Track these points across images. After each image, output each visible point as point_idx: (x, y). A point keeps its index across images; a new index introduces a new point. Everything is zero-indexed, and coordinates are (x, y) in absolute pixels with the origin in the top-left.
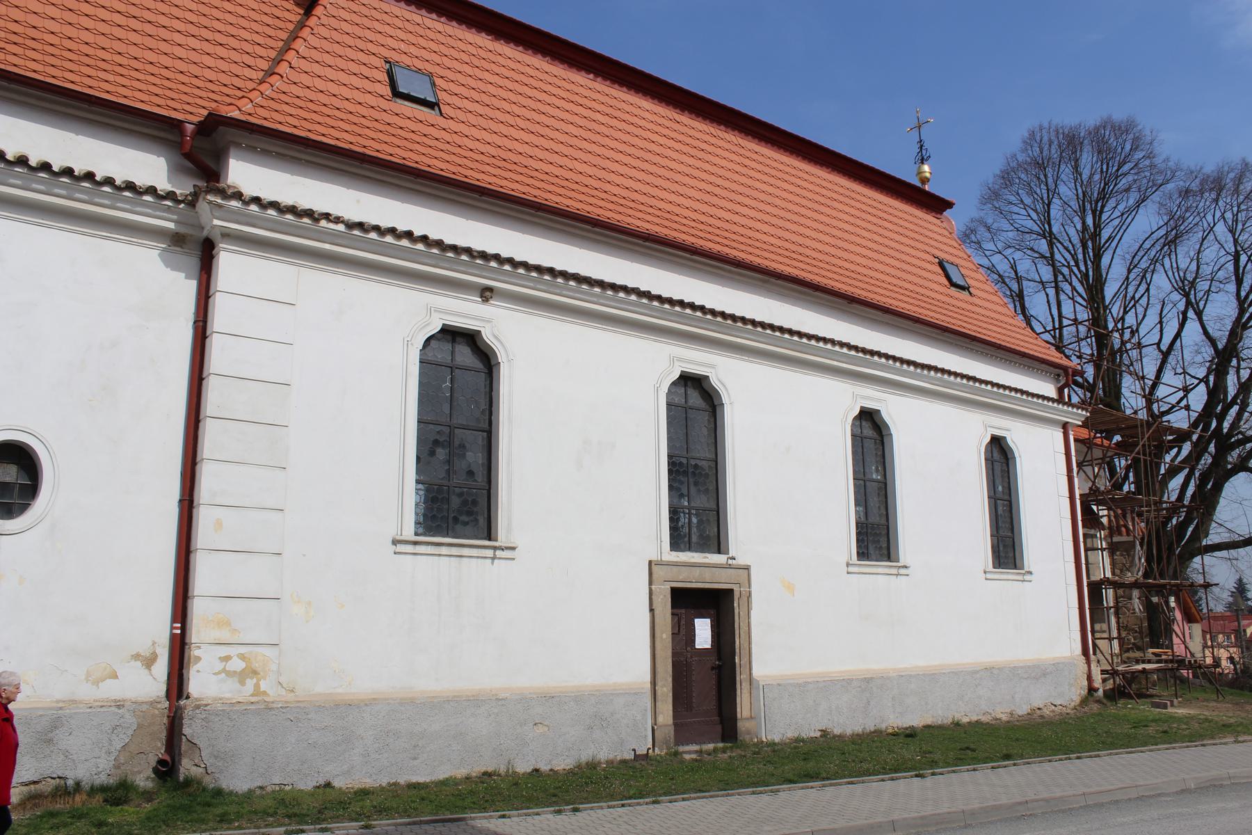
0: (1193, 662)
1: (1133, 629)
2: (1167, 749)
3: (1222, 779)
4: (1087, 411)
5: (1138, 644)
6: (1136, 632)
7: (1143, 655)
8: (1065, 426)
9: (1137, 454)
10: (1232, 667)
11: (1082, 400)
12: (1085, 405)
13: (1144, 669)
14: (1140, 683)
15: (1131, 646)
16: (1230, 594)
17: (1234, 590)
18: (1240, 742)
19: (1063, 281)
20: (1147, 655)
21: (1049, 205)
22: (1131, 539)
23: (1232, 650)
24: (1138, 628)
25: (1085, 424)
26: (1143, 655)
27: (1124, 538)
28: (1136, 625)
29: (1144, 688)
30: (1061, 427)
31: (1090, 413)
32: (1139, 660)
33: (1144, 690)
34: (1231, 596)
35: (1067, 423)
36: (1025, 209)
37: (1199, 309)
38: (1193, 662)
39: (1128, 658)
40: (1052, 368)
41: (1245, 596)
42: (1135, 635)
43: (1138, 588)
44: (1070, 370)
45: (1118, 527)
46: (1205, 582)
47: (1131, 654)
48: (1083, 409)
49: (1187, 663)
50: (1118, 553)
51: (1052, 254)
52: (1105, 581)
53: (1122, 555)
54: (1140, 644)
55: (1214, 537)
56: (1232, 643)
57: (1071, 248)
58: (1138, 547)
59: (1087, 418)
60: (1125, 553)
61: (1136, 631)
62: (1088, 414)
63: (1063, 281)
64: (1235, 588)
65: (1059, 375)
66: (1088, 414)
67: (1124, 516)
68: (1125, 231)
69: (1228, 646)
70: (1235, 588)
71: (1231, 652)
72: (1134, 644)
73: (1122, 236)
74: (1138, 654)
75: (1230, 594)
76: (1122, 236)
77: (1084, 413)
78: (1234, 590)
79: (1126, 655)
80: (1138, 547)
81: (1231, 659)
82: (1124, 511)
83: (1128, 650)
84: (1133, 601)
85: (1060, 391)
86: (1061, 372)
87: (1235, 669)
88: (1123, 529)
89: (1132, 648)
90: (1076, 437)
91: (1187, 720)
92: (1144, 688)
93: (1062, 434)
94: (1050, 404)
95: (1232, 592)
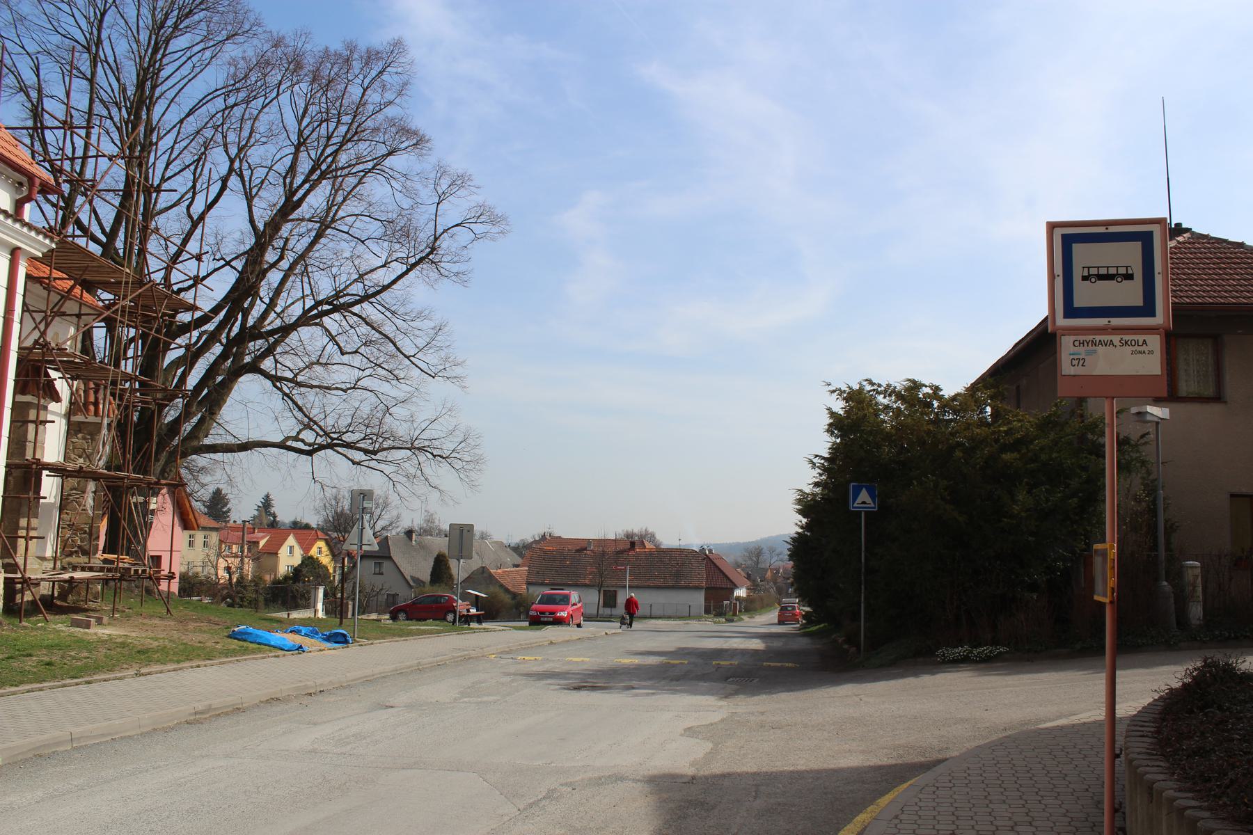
0: (140, 572)
1: (82, 529)
2: (28, 691)
3: (58, 744)
4: (52, 240)
5: (85, 547)
6: (85, 532)
7: (87, 560)
8: (15, 252)
9: (113, 313)
10: (227, 576)
11: (50, 227)
12: (53, 233)
13: (72, 578)
14: (79, 594)
15: (76, 549)
16: (256, 508)
17: (261, 505)
18: (143, 675)
19: (106, 118)
20: (92, 561)
21: (103, 15)
22: (98, 420)
23: (230, 560)
24: (89, 528)
25: (47, 258)
26: (87, 560)
27: (92, 419)
28: (86, 524)
29: (82, 601)
30: (9, 251)
31: (56, 244)
32: (77, 566)
33: (82, 603)
34: (257, 510)
35: (19, 248)
36: (69, 6)
37: (251, 194)
38: (140, 572)
39: (69, 564)
40: (10, 170)
41: (269, 511)
42: (83, 536)
43: (95, 479)
44: (37, 181)
45: (86, 404)
46: (34, 458)
47: (74, 559)
48: (46, 236)
49: (132, 572)
50: (80, 436)
51: (94, 74)
52: (34, 463)
53: (84, 438)
54: (87, 548)
55: (214, 437)
56: (232, 553)
57: (115, 68)
58: (104, 431)
59: (52, 251)
60: (89, 437)
61: (86, 531)
62: (54, 246)
63: (106, 118)
64: (262, 502)
65: (21, 184)
66: (54, 246)
67: (96, 392)
68: (190, 81)
69: (228, 557)
70: (262, 502)
71: (230, 562)
72: (79, 547)
73: (185, 85)
74: (83, 560)
75: (256, 508)
76: (185, 85)
77: (47, 241)
78: (261, 505)
79: (68, 559)
80: (104, 431)
81: (228, 569)
82: (97, 385)
83: (70, 554)
84: (86, 495)
85: (19, 205)
86: (24, 180)
87: (230, 579)
88: (92, 408)
89: (76, 552)
90: (30, 272)
91: (107, 642)
92: (82, 601)
93: (8, 262)
94: (33, 234)
95: (259, 507)
